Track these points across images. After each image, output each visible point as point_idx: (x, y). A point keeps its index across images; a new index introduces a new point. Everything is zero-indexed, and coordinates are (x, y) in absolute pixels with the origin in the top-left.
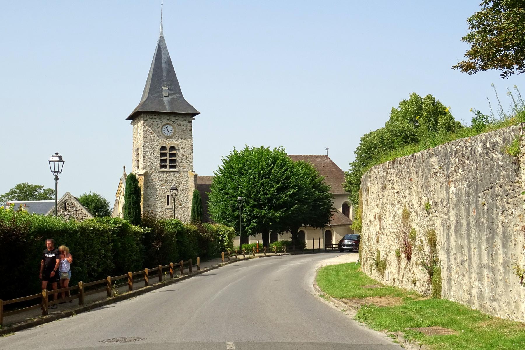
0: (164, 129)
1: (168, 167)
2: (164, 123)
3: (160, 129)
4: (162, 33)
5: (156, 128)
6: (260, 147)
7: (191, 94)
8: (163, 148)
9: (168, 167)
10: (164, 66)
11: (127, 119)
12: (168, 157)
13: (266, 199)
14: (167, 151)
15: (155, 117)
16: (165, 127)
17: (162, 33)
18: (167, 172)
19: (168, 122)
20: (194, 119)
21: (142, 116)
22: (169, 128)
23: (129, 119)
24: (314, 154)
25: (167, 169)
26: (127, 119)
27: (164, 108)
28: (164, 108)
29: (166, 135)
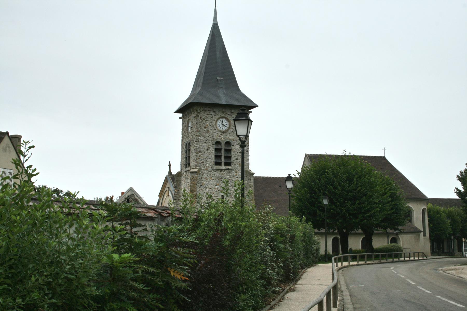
0: (219, 123)
1: (223, 164)
2: (218, 117)
3: (214, 122)
4: (215, 18)
5: (211, 121)
6: (181, 120)
7: (247, 84)
8: (218, 143)
9: (223, 164)
10: (218, 54)
11: (175, 112)
12: (223, 153)
13: (267, 260)
14: (223, 147)
15: (210, 109)
16: (219, 121)
17: (215, 18)
18: (221, 170)
19: (223, 115)
20: (251, 112)
21: (195, 108)
22: (225, 122)
23: (178, 112)
24: (181, 146)
25: (223, 167)
26: (175, 112)
27: (217, 101)
28: (217, 101)
29: (221, 129)
